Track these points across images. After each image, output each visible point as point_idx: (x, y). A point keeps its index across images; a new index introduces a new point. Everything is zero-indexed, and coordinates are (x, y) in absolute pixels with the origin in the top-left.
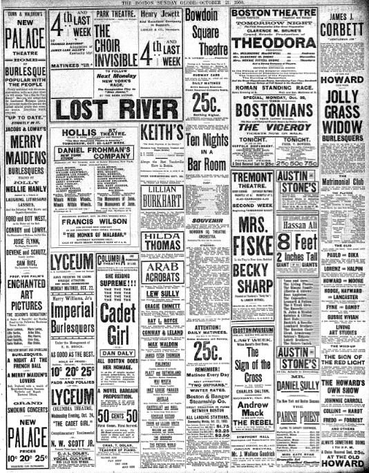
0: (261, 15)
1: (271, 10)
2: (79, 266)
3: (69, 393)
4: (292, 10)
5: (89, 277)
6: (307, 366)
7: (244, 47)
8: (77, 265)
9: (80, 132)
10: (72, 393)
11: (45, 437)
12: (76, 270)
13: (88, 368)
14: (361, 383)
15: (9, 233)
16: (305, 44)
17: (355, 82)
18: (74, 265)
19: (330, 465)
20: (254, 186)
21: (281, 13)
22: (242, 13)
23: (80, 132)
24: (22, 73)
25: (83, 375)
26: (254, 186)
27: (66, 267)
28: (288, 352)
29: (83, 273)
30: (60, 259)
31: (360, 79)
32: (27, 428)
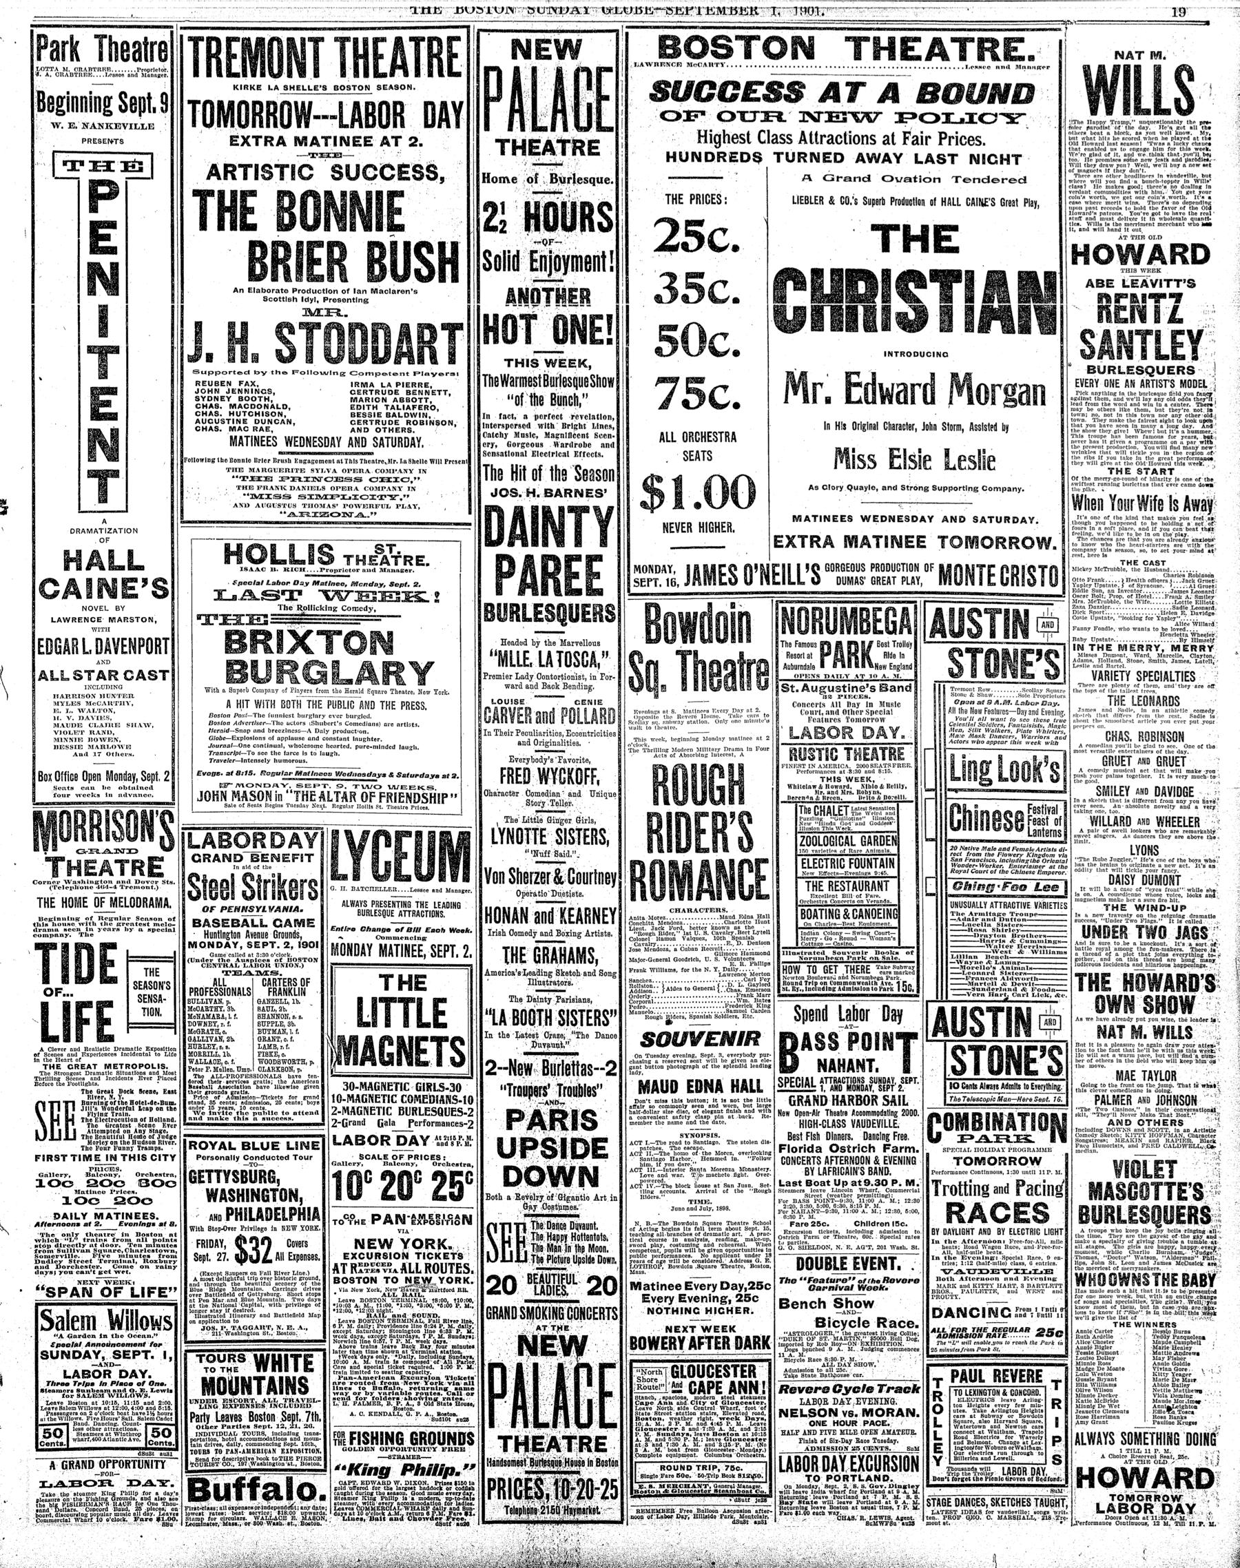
2: (424, 872)
3: (388, 845)
4: (927, 38)
5: (456, 905)
6: (1033, 1067)
7: (907, 249)
8: (418, 868)
11: (610, 1394)
12: (415, 883)
13: (453, 1174)
15: (494, 926)
16: (966, 1214)
18: (408, 867)
19: (1097, 259)
21: (517, 1445)
22: (696, 47)
23: (282, 553)
25: (436, 1197)
27: (382, 871)
28: (964, 1023)
29: (434, 891)
30: (362, 847)
31: (1200, 254)
32: (548, 1366)
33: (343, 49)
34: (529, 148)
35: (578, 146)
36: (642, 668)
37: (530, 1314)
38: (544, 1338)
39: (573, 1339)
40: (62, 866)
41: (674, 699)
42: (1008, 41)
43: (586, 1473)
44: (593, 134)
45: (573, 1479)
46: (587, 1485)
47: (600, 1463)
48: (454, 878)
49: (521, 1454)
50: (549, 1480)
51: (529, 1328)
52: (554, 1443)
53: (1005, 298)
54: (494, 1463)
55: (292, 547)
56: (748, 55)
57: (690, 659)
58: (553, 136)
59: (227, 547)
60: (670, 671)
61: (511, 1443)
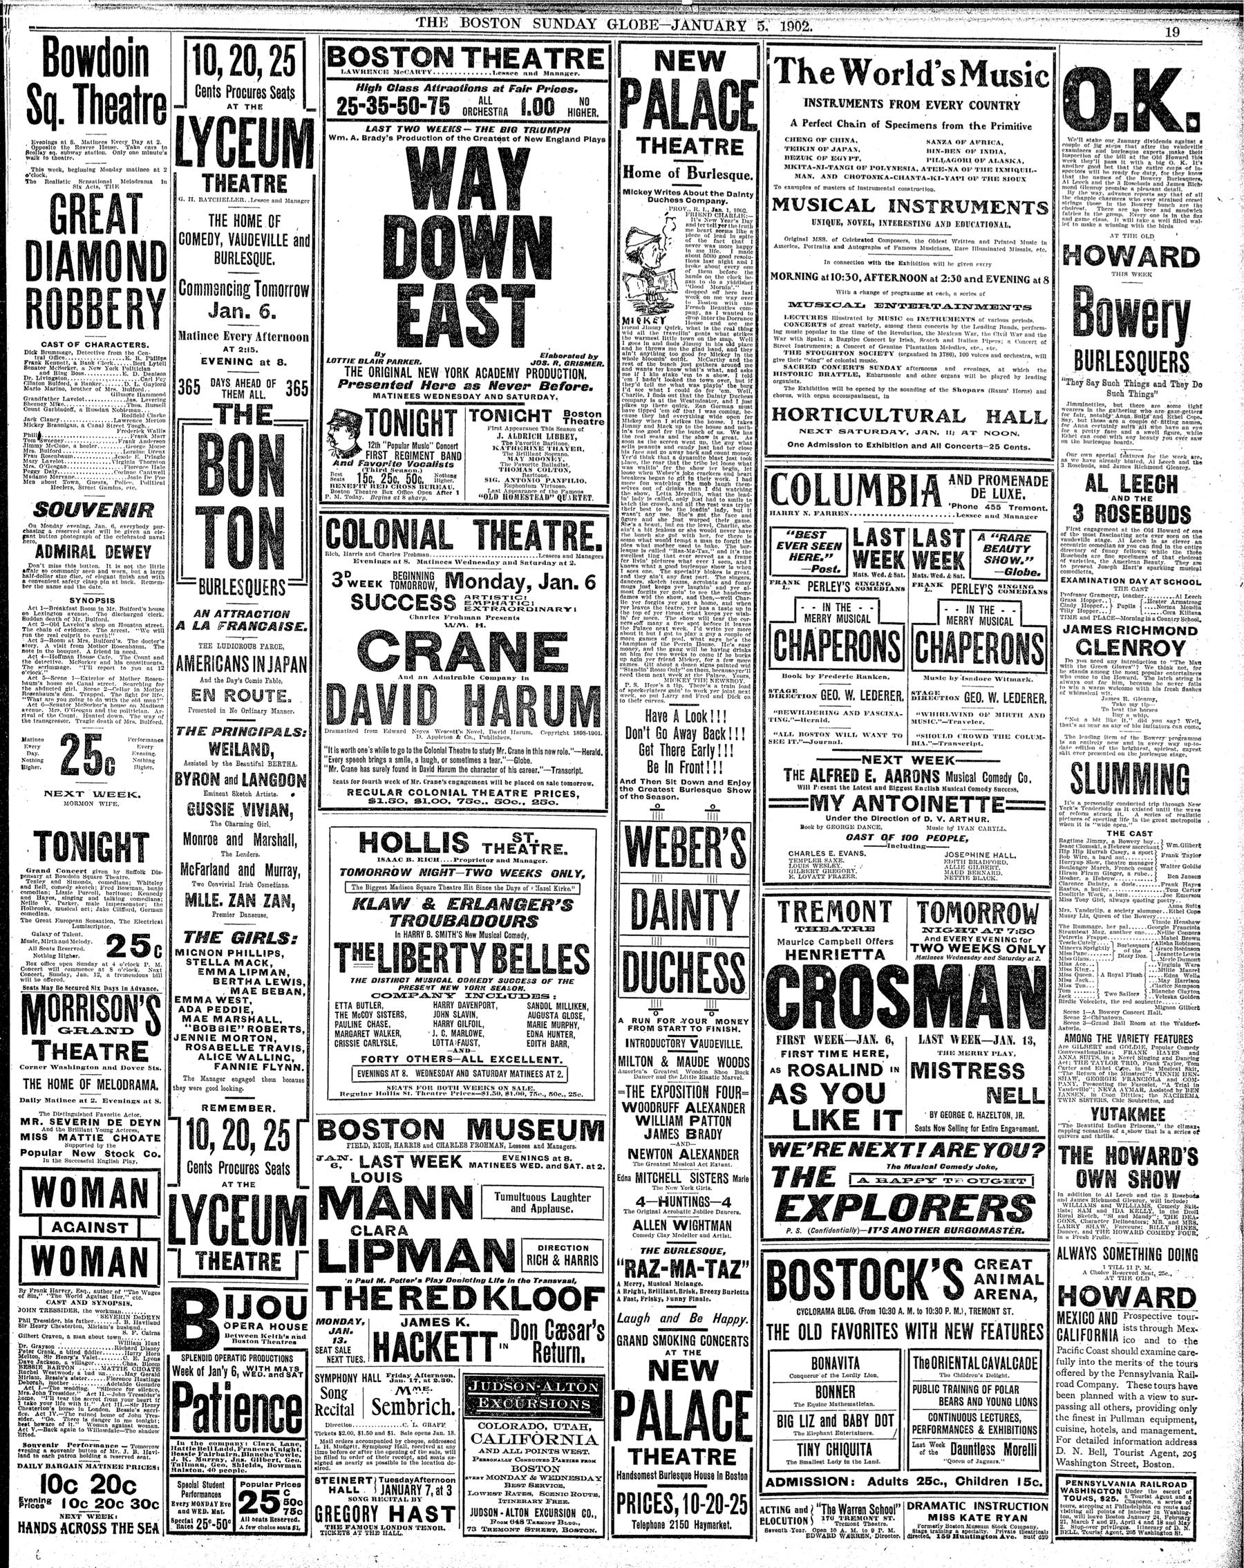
0: (427, 63)
1: (457, 47)
4: (524, 49)
9: (418, 841)
10: (236, 1209)
14: (1185, 1156)
17: (1175, 264)
20: (100, 1052)
21: (647, 1457)
22: (359, 56)
23: (418, 841)
24: (1113, 365)
26: (100, 1052)
31: (1190, 257)
33: (481, 531)
34: (671, 146)
35: (721, 146)
36: (40, 101)
37: (661, 1341)
38: (676, 1363)
39: (705, 1363)
40: (48, 1050)
41: (71, 131)
42: (584, 524)
43: (714, 1486)
44: (737, 133)
45: (702, 1493)
46: (717, 1498)
47: (729, 1476)
48: (585, 724)
49: (652, 1467)
50: (678, 1494)
51: (659, 1354)
52: (683, 1456)
53: (993, 992)
54: (623, 1476)
55: (427, 835)
56: (554, 65)
57: (87, 92)
58: (695, 135)
59: (362, 835)
60: (67, 106)
61: (641, 1456)
